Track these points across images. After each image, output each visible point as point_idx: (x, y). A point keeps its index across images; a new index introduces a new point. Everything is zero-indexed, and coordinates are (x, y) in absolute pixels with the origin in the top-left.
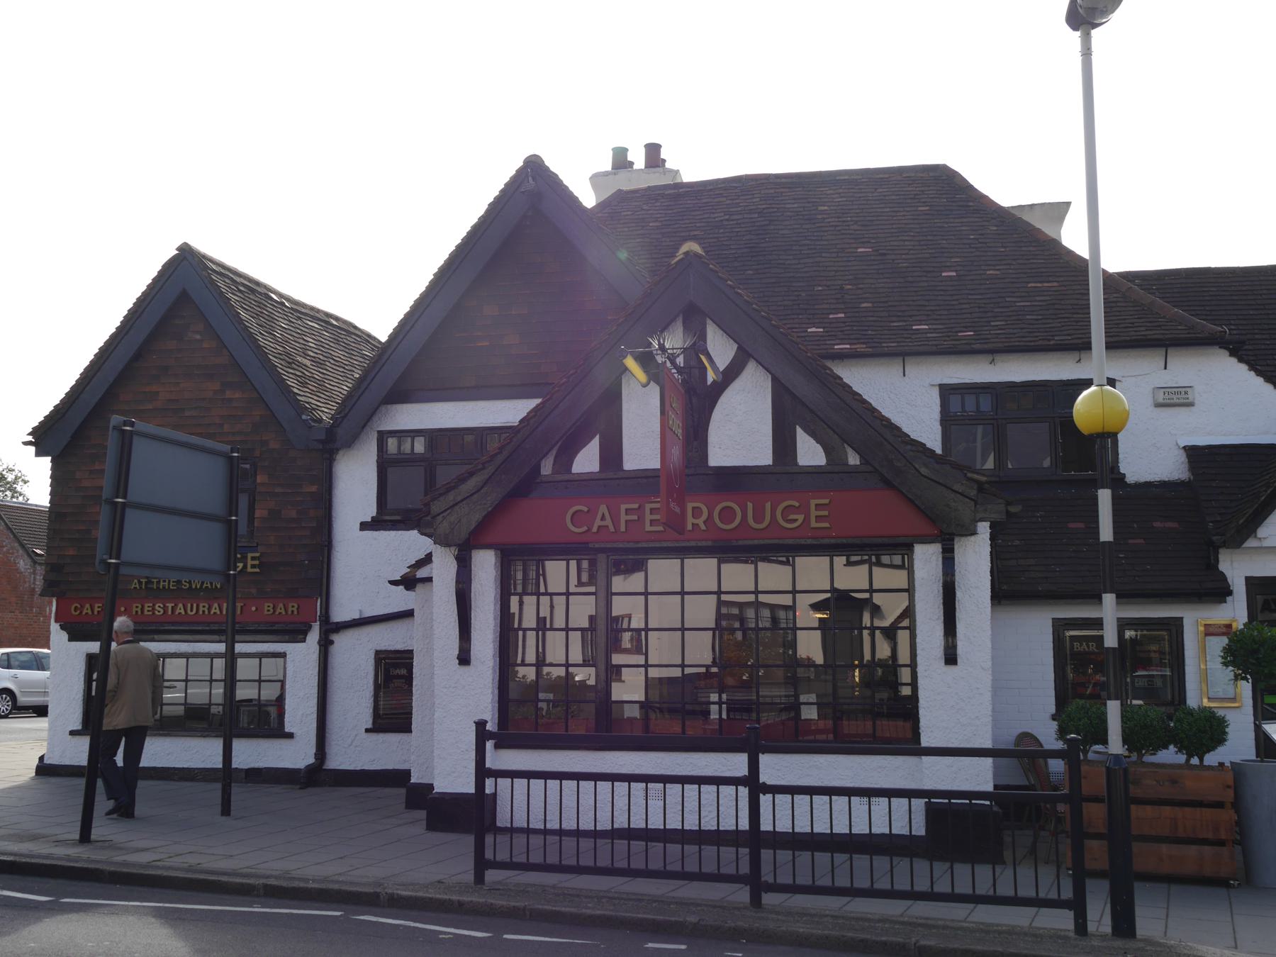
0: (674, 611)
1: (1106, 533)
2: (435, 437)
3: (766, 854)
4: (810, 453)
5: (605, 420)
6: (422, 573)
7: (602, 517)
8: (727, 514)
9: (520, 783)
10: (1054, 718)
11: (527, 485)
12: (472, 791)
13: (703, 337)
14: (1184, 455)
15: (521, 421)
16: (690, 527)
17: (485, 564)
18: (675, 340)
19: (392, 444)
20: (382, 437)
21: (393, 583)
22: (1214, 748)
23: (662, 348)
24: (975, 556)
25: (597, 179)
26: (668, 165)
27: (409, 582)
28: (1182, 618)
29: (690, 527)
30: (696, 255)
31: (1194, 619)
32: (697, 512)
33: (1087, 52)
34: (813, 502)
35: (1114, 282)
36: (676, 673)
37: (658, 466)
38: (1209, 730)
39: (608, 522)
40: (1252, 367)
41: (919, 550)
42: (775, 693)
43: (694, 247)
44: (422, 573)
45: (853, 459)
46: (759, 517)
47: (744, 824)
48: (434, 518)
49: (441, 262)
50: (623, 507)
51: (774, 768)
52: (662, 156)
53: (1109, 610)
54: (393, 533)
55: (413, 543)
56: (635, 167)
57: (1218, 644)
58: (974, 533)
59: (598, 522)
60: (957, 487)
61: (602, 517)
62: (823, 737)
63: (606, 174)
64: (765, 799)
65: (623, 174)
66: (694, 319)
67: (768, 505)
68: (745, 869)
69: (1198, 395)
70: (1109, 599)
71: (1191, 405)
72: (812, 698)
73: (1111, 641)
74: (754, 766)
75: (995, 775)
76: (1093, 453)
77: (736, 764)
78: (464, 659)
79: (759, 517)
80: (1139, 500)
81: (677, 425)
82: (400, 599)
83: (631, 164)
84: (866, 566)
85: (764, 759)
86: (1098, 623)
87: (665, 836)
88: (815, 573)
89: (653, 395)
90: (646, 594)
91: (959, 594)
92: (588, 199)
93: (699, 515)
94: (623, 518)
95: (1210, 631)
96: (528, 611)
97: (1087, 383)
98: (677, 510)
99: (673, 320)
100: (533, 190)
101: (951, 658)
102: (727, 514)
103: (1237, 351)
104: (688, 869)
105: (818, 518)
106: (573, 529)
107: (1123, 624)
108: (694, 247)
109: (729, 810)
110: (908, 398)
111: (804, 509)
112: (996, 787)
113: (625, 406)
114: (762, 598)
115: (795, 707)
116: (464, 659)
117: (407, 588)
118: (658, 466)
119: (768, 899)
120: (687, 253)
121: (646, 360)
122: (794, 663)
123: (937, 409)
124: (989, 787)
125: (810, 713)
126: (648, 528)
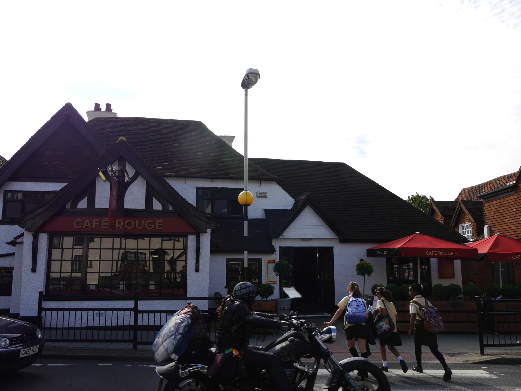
0: (104, 256)
1: (246, 234)
2: (26, 194)
3: (139, 333)
4: (157, 206)
5: (90, 191)
6: (19, 240)
7: (87, 223)
8: (129, 224)
9: (54, 313)
10: (225, 288)
11: (61, 211)
12: (37, 315)
13: (125, 167)
14: (264, 212)
15: (60, 190)
16: (117, 228)
17: (44, 238)
18: (115, 168)
19: (9, 195)
20: (6, 193)
21: (7, 243)
22: (270, 295)
23: (112, 170)
24: (206, 240)
25: (89, 113)
26: (113, 111)
27: (13, 243)
28: (262, 258)
29: (117, 228)
30: (124, 141)
31: (265, 258)
32: (119, 223)
33: (246, 95)
34: (157, 221)
35: (250, 160)
36: (110, 275)
37: (108, 207)
38: (269, 290)
39: (89, 225)
40: (282, 188)
41: (190, 237)
42: (141, 281)
43: (124, 139)
44: (19, 240)
45: (171, 208)
46: (140, 225)
47: (132, 323)
48: (26, 221)
49: (32, 135)
50: (94, 220)
51: (143, 305)
52: (112, 108)
53: (246, 256)
54: (7, 226)
55: (15, 230)
56: (102, 110)
57: (272, 266)
58: (206, 232)
59: (85, 225)
60: (202, 218)
61: (87, 223)
62: (156, 295)
63: (92, 112)
64: (140, 315)
65: (98, 112)
66: (122, 161)
67: (143, 222)
68: (132, 338)
69: (268, 195)
70: (246, 253)
71: (266, 197)
72: (153, 283)
73: (246, 265)
74: (136, 305)
75: (209, 305)
76: (240, 209)
77: (130, 304)
78: (34, 270)
79: (140, 225)
80: (253, 223)
81: (115, 194)
82: (10, 249)
83: (101, 109)
84: (173, 241)
85: (140, 302)
86: (242, 260)
87: (105, 328)
88: (156, 243)
89: (108, 185)
90: (100, 249)
91: (201, 251)
92: (86, 119)
93: (119, 224)
94: (94, 224)
95: (269, 262)
96: (56, 253)
97: (242, 190)
98: (113, 222)
99: (115, 161)
100: (68, 113)
101: (197, 270)
102: (129, 224)
103: (279, 183)
104: (113, 338)
105: (159, 226)
106: (132, 221)
107: (249, 260)
108: (124, 139)
109: (128, 319)
110: (187, 190)
111: (155, 223)
112: (209, 309)
113: (97, 187)
114: (139, 251)
115: (148, 285)
116: (34, 270)
117: (13, 245)
118: (108, 207)
119: (139, 347)
120: (121, 140)
121: (105, 173)
122: (146, 273)
123: (195, 194)
124: (207, 309)
125: (152, 287)
126: (103, 227)
